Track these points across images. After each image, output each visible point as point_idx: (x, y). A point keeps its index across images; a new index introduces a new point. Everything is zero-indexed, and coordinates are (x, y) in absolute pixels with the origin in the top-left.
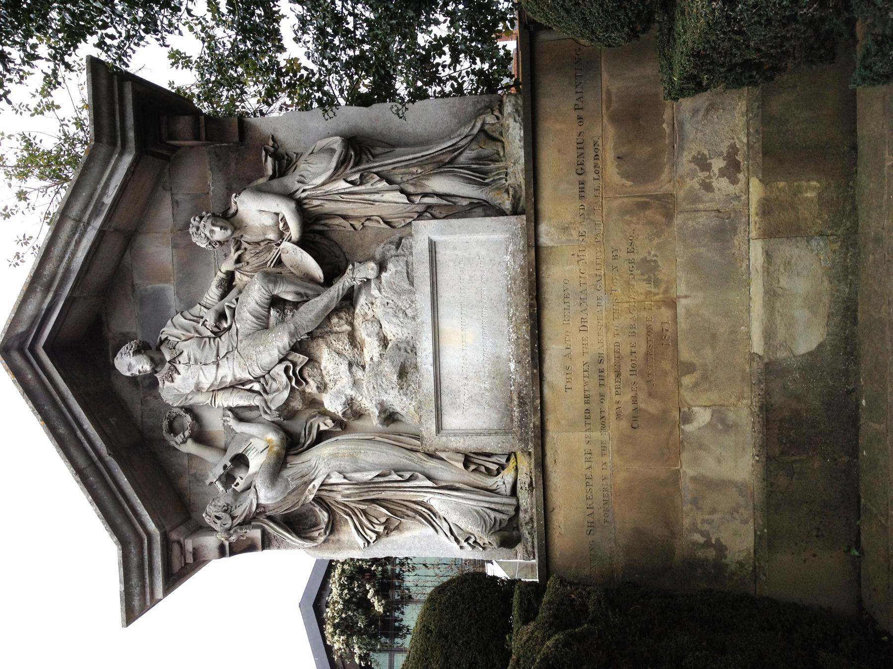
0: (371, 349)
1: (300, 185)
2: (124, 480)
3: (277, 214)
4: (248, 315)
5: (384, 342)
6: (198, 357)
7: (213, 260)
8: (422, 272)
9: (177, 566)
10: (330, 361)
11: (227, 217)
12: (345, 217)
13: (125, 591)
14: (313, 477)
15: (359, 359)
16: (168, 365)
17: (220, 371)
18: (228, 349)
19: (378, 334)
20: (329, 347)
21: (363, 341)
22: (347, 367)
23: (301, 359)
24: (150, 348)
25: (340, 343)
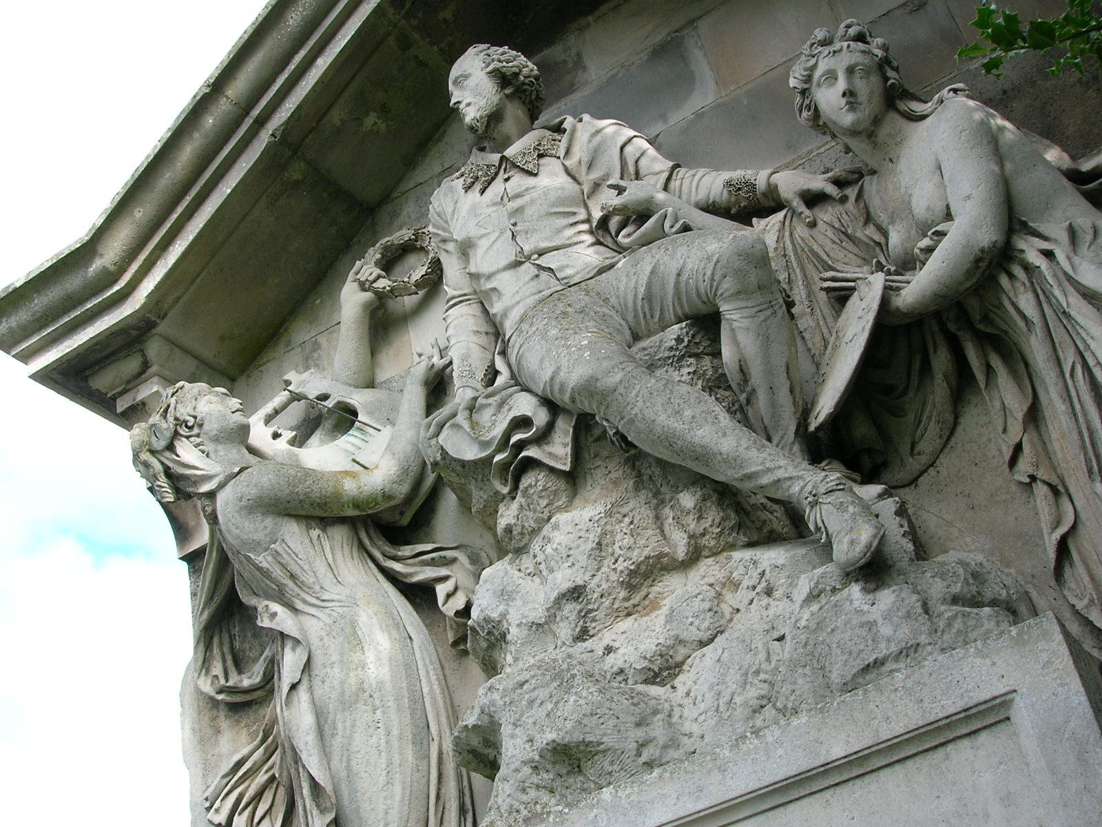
0: (632, 640)
1: (1064, 237)
2: (226, 188)
3: (948, 216)
4: (649, 268)
5: (663, 670)
6: (529, 212)
7: (805, 150)
8: (894, 710)
9: (103, 381)
10: (578, 532)
11: (895, 95)
12: (1034, 415)
13: (16, 290)
14: (299, 605)
15: (600, 614)
16: (495, 158)
17: (507, 275)
18: (562, 268)
19: (681, 642)
20: (609, 514)
21: (655, 606)
22: (567, 585)
23: (559, 451)
24: (527, 99)
25: (627, 541)
